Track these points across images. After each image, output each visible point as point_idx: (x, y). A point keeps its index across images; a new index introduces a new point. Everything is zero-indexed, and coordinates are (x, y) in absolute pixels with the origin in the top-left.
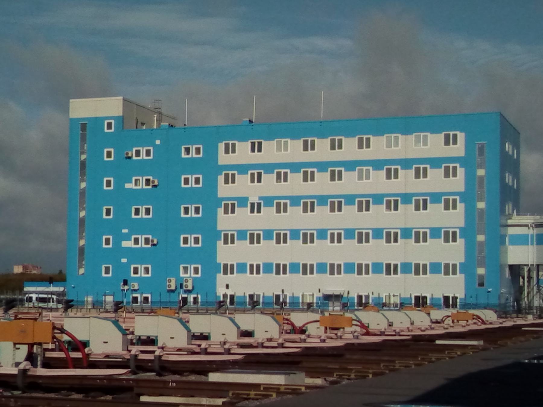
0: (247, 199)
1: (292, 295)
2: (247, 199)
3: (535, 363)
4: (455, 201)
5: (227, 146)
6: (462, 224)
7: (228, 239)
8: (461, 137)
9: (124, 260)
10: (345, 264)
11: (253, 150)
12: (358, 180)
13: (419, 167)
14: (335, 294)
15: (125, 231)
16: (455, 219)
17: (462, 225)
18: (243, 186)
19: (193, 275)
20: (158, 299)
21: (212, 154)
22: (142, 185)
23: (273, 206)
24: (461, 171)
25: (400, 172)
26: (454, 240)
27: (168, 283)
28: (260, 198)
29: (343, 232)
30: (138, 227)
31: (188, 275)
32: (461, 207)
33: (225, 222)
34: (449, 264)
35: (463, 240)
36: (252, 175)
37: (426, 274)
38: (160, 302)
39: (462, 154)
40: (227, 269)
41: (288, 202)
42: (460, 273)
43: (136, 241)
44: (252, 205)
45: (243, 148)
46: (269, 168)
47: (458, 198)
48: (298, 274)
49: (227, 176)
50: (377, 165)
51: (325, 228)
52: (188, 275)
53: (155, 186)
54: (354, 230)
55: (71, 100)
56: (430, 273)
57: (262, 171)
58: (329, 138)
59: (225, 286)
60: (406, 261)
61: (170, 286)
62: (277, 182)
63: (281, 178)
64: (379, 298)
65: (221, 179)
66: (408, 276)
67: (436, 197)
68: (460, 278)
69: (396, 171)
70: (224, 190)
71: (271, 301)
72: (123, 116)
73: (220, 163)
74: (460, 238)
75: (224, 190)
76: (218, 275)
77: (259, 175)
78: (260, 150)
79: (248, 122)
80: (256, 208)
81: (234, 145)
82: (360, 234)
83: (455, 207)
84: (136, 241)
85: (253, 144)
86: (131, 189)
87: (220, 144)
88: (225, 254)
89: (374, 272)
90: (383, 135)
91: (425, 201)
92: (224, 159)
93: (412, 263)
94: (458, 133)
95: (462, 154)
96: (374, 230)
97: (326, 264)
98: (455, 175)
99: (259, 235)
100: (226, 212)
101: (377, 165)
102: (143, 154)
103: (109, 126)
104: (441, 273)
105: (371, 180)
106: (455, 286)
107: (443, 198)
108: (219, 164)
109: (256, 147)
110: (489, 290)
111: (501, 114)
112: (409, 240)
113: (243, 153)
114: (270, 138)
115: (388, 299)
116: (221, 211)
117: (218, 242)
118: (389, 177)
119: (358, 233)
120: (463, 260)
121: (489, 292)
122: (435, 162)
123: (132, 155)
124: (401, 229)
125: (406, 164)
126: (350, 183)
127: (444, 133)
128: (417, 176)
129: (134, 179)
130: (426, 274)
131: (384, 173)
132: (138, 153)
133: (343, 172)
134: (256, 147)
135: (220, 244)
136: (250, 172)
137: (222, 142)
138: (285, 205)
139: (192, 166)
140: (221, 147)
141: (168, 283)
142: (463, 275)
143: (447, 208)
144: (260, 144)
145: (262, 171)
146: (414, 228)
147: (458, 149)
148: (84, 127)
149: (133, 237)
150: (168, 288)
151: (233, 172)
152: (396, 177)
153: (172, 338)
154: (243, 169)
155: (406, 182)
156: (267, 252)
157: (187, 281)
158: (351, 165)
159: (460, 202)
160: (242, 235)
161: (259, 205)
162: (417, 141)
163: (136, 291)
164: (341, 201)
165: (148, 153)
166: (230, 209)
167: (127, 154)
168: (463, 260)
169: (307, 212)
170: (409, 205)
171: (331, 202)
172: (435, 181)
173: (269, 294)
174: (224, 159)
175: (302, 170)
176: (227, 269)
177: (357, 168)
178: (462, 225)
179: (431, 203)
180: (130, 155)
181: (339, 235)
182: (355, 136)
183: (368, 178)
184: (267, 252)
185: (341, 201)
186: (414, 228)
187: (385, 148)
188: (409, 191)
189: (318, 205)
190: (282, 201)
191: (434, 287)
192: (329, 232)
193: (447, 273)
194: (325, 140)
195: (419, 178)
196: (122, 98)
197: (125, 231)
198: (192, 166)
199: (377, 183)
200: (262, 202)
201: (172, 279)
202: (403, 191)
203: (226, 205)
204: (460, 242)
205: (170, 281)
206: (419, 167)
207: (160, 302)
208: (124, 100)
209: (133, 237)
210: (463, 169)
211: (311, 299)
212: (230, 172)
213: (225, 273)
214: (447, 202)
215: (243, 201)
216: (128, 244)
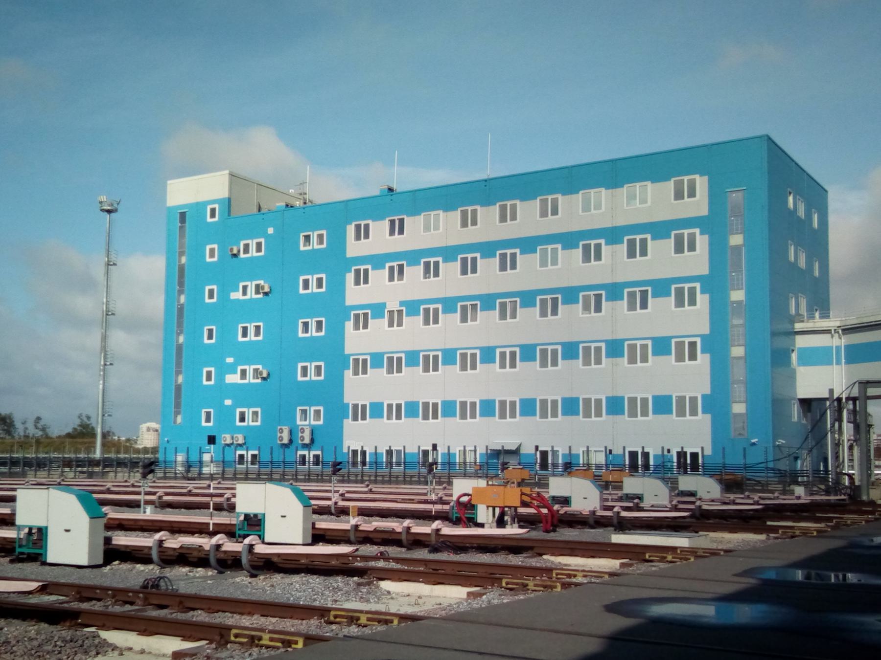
0: (384, 305)
1: (567, 452)
2: (384, 305)
3: (851, 571)
4: (692, 291)
5: (358, 227)
6: (705, 329)
7: (361, 367)
8: (701, 183)
9: (228, 402)
10: (656, 398)
11: (392, 233)
12: (628, 258)
13: (633, 238)
14: (506, 448)
15: (230, 360)
16: (695, 319)
17: (706, 330)
18: (380, 289)
19: (313, 423)
20: (742, 462)
21: (339, 242)
22: (251, 294)
23: (456, 312)
24: (702, 242)
25: (604, 249)
26: (693, 357)
27: (279, 435)
28: (402, 303)
29: (517, 350)
30: (246, 354)
31: (307, 423)
32: (702, 300)
33: (357, 342)
34: (684, 397)
35: (707, 356)
36: (391, 269)
37: (437, 418)
38: (272, 462)
39: (704, 211)
40: (359, 412)
41: (440, 306)
42: (703, 412)
43: (244, 373)
44: (391, 312)
45: (379, 228)
46: (413, 257)
47: (698, 286)
48: (533, 418)
49: (357, 272)
50: (568, 240)
51: (491, 345)
52: (307, 423)
53: (266, 294)
54: (383, 354)
55: (169, 182)
56: (481, 415)
57: (405, 263)
58: (459, 210)
59: (359, 437)
60: (615, 395)
61: (281, 439)
62: (425, 277)
63: (591, 254)
64: (570, 454)
65: (350, 277)
66: (618, 418)
67: (661, 287)
68: (703, 421)
69: (598, 247)
70: (355, 295)
71: (620, 462)
72: (229, 199)
73: (349, 254)
74: (703, 352)
75: (355, 295)
76: (345, 421)
77: (401, 268)
78: (401, 232)
79: (387, 190)
80: (395, 319)
81: (367, 227)
82: (544, 352)
83: (693, 302)
84: (244, 373)
85: (392, 222)
86: (238, 300)
87: (348, 227)
88: (357, 389)
89: (609, 413)
90: (578, 193)
91: (598, 298)
92: (354, 248)
93: (455, 402)
94: (697, 177)
95: (704, 211)
96: (522, 347)
97: (623, 398)
98: (692, 248)
99: (436, 358)
100: (357, 327)
101: (568, 240)
102: (252, 249)
103: (213, 212)
104: (455, 416)
105: (559, 266)
106: (694, 434)
107: (353, 313)
108: (348, 256)
109: (397, 227)
110: (753, 441)
111: (769, 139)
112: (619, 360)
113: (380, 239)
114: (415, 212)
115: (462, 457)
116: (349, 325)
117: (346, 372)
118: (587, 258)
119: (388, 358)
120: (708, 391)
121: (754, 444)
122: (659, 230)
123: (239, 251)
124: (606, 341)
125: (613, 235)
126: (530, 272)
127: (673, 180)
128: (631, 254)
129: (241, 285)
130: (437, 418)
131: (579, 252)
132: (246, 249)
133: (698, 237)
134: (397, 227)
135: (349, 374)
136: (388, 265)
137: (351, 224)
138: (436, 311)
139: (313, 262)
140: (351, 230)
141: (279, 435)
142: (708, 417)
143: (680, 303)
144: (402, 221)
145: (405, 263)
146: (353, 355)
147: (698, 205)
148: (183, 216)
149: (239, 368)
150: (279, 442)
151: (513, 251)
152: (598, 257)
153: (283, 517)
154: (378, 261)
155: (615, 266)
156: (412, 385)
157: (303, 431)
158: (529, 245)
159: (702, 292)
160: (377, 359)
161: (400, 312)
162: (631, 197)
163: (240, 445)
164: (557, 298)
165: (259, 247)
166: (361, 322)
167: (232, 250)
168: (708, 391)
169: (429, 324)
170: (619, 302)
171: (541, 300)
172: (661, 260)
173: (412, 449)
174: (354, 248)
175: (423, 260)
176: (359, 412)
177: (539, 248)
178: (706, 330)
179: (653, 296)
180: (235, 252)
181: (513, 354)
182: (456, 209)
183: (555, 262)
184: (412, 385)
185: (557, 298)
186: (353, 355)
187: (581, 213)
188: (620, 279)
189: (563, 304)
190: (432, 307)
191: (662, 436)
192: (498, 351)
193: (681, 413)
194: (491, 208)
195: (359, 284)
196: (227, 172)
197: (230, 360)
198: (313, 262)
199: (570, 268)
200: (404, 309)
201: (283, 428)
202: (608, 280)
203: (357, 316)
204: (703, 360)
205: (281, 431)
206: (633, 238)
207: (272, 462)
208: (232, 175)
209: (239, 368)
210: (706, 237)
211: (473, 456)
212: (432, 260)
213: (355, 418)
214: (680, 293)
215: (378, 310)
216: (233, 378)
